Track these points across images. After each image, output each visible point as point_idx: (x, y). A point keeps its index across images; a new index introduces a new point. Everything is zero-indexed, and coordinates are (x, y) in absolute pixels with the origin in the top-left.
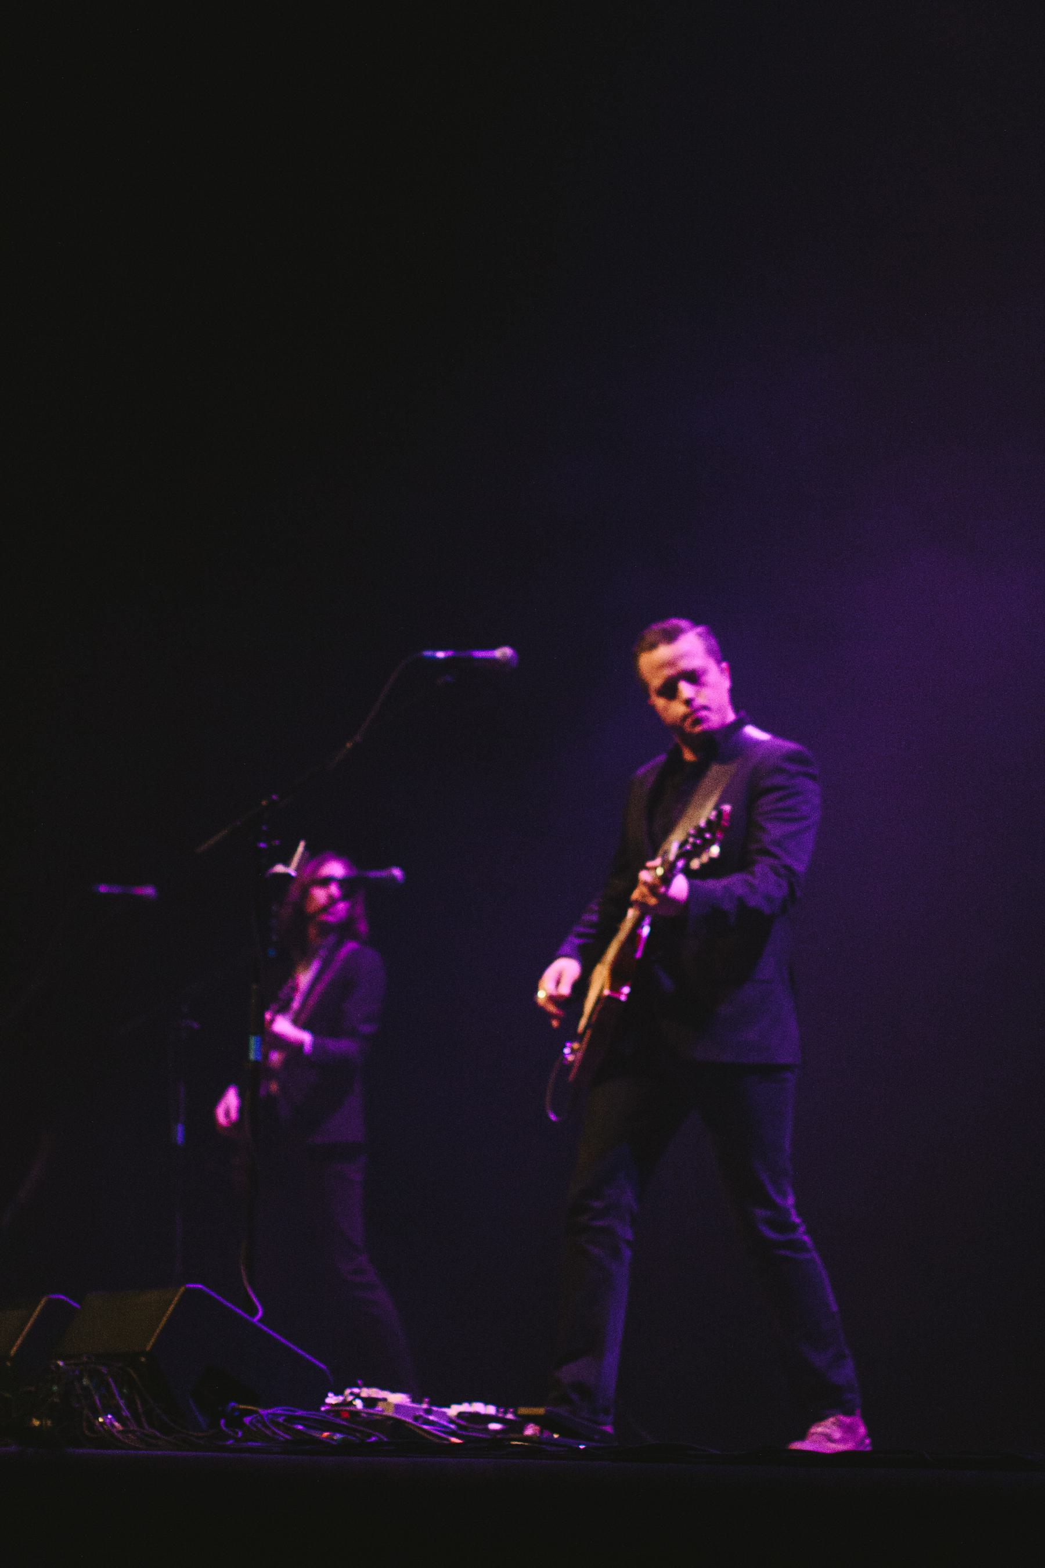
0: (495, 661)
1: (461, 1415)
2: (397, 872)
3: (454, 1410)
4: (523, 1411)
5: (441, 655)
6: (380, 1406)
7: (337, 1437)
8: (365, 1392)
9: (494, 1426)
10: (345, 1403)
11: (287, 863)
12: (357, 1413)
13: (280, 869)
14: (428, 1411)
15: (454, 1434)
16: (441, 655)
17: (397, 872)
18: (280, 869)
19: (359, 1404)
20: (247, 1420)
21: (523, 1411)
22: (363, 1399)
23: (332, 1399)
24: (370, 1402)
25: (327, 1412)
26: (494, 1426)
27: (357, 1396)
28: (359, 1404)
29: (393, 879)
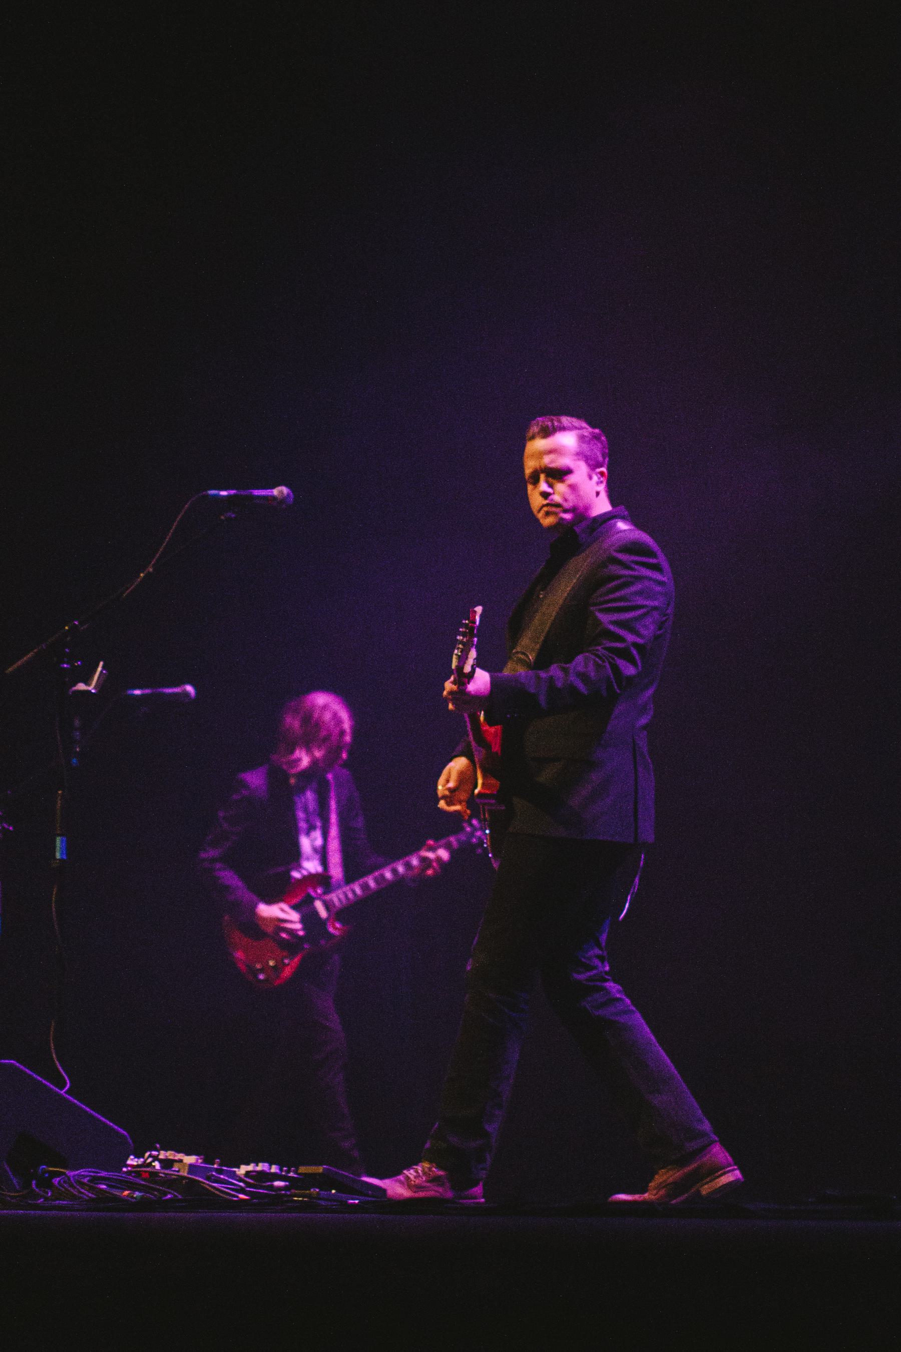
0: (274, 498)
1: (248, 1173)
2: (189, 688)
3: (242, 1170)
4: (302, 1169)
5: (224, 493)
6: (176, 1167)
7: (137, 1194)
8: (162, 1155)
9: (277, 1183)
10: (145, 1165)
11: (87, 683)
12: (155, 1174)
13: (81, 687)
14: (219, 1171)
15: (242, 1191)
16: (224, 493)
17: (189, 688)
18: (81, 687)
19: (157, 1164)
20: (56, 1181)
21: (302, 1169)
22: (160, 1161)
23: (132, 1161)
24: (167, 1164)
25: (128, 1172)
26: (277, 1183)
27: (156, 1158)
28: (157, 1164)
29: (187, 694)
